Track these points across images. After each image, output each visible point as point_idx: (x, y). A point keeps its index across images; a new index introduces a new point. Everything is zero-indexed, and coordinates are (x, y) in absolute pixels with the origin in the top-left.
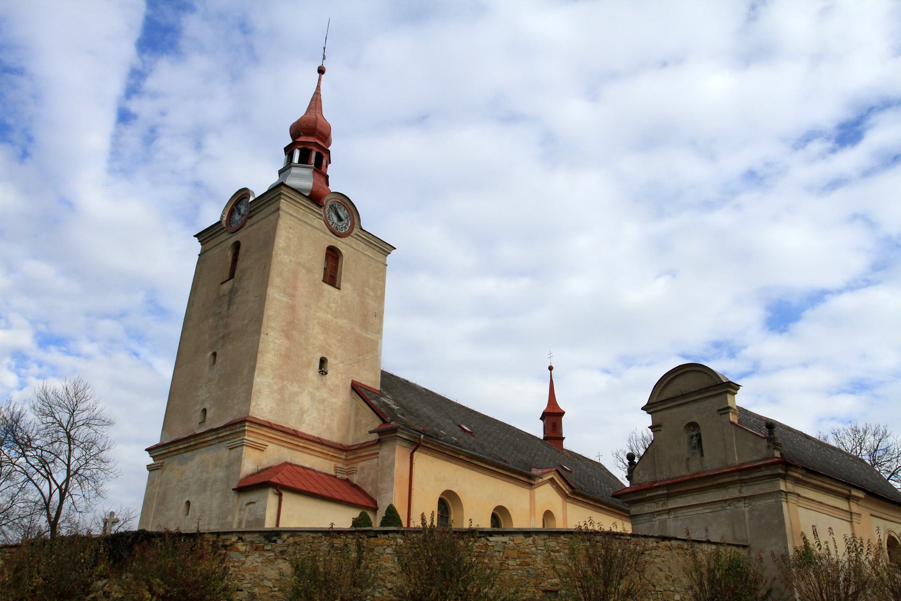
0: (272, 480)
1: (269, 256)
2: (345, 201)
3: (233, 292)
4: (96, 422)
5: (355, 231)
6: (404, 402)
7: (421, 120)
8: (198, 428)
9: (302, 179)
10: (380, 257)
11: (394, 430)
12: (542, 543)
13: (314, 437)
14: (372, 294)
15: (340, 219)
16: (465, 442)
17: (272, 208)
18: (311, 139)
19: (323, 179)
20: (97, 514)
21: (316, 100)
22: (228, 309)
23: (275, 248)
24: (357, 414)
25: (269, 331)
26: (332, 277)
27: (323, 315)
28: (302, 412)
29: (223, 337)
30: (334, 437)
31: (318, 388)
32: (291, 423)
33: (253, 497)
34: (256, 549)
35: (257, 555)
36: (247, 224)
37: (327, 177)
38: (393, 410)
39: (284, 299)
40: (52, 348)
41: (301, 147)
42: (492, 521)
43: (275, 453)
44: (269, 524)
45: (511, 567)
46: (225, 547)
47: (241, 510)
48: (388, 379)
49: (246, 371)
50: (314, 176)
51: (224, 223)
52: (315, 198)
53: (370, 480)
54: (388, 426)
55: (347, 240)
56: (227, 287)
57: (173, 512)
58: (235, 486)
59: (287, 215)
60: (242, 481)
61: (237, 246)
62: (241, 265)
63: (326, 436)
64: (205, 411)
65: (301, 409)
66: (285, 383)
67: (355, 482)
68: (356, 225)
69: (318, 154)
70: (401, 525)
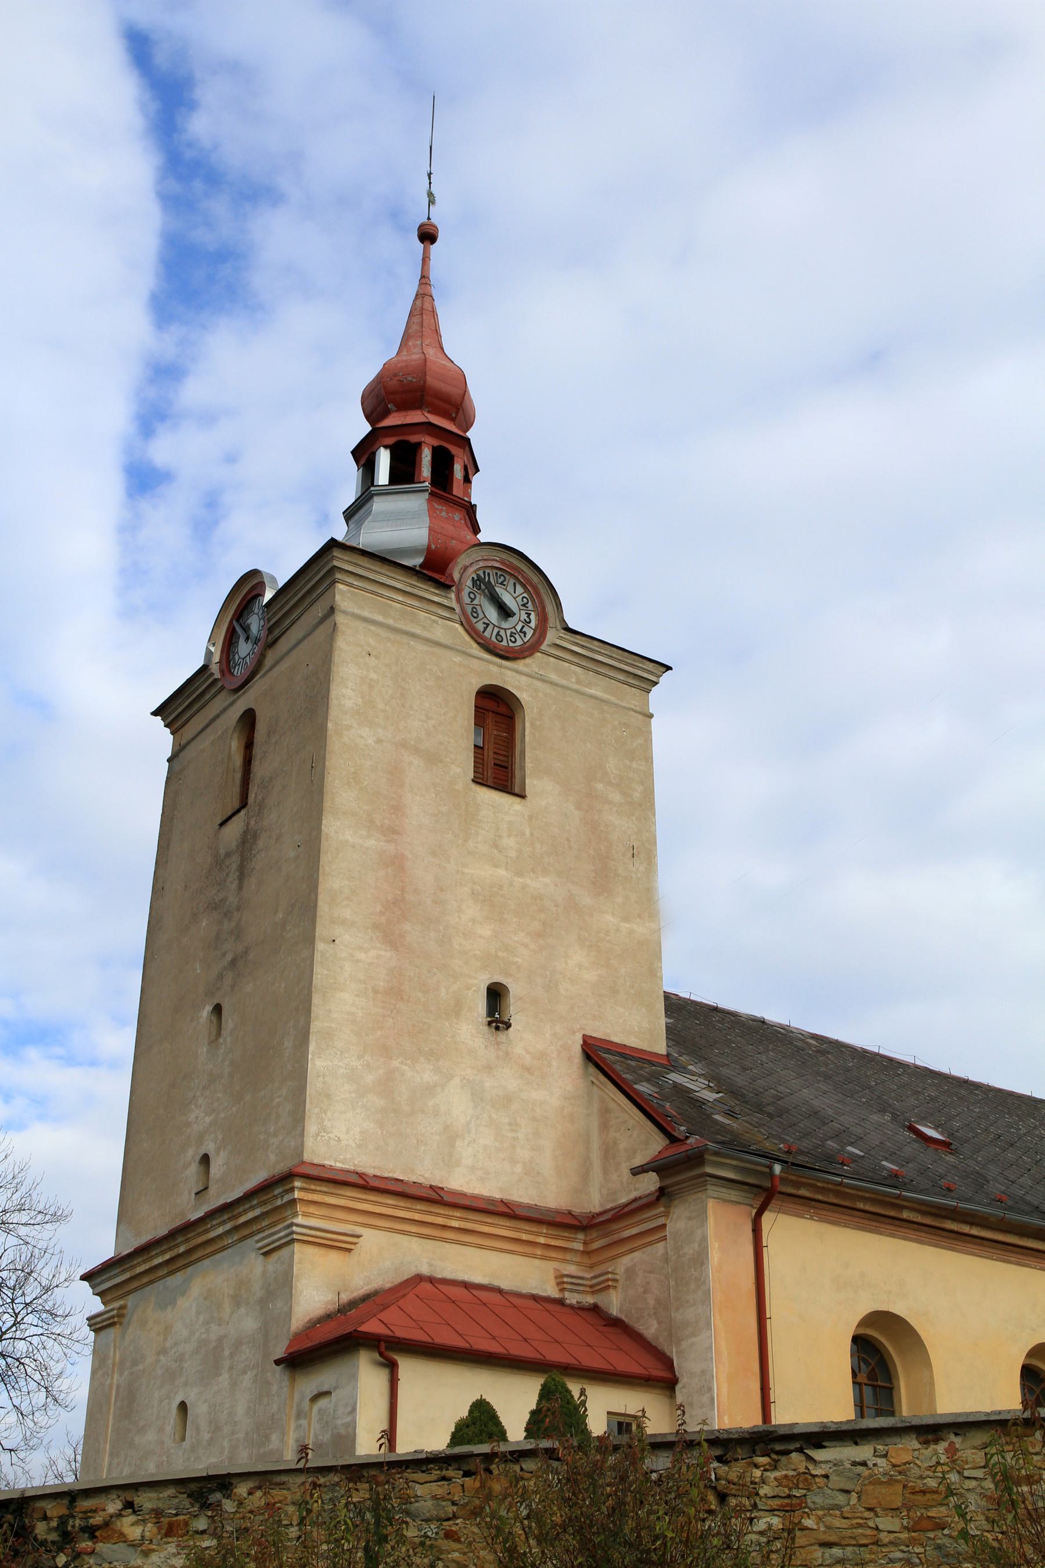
0: (364, 1328)
1: (320, 736)
2: (517, 565)
3: (248, 840)
4: (24, 1217)
5: (551, 636)
6: (741, 1080)
7: (870, 362)
8: (195, 1208)
9: (405, 522)
10: (630, 696)
11: (696, 1159)
12: (979, 1457)
13: (490, 1201)
14: (616, 797)
15: (505, 612)
16: (923, 1171)
17: (318, 610)
18: (416, 417)
19: (458, 516)
20: (54, 1454)
21: (423, 318)
22: (240, 888)
23: (334, 712)
24: (604, 1126)
25: (337, 931)
26: (498, 767)
27: (484, 872)
28: (451, 1136)
29: (233, 962)
30: (550, 1193)
31: (489, 1068)
32: (424, 1171)
33: (323, 1378)
34: (170, 1531)
35: (172, 1549)
36: (268, 662)
37: (470, 511)
38: (699, 1104)
39: (371, 843)
40: (32, 1053)
41: (390, 441)
42: (1023, 1386)
43: (385, 1255)
44: (367, 1445)
45: (885, 1538)
46: (91, 1532)
47: (299, 1415)
48: (688, 1019)
49: (288, 1044)
50: (431, 511)
51: (215, 669)
52: (434, 569)
53: (652, 1302)
54: (683, 1148)
55: (531, 664)
56: (236, 827)
57: (151, 1436)
58: (280, 1352)
59: (361, 625)
60: (297, 1337)
61: (249, 719)
62: (260, 770)
63: (523, 1195)
64: (205, 1160)
65: (446, 1127)
66: (396, 1063)
67: (614, 1311)
68: (552, 620)
69: (436, 452)
70: (502, 1435)
